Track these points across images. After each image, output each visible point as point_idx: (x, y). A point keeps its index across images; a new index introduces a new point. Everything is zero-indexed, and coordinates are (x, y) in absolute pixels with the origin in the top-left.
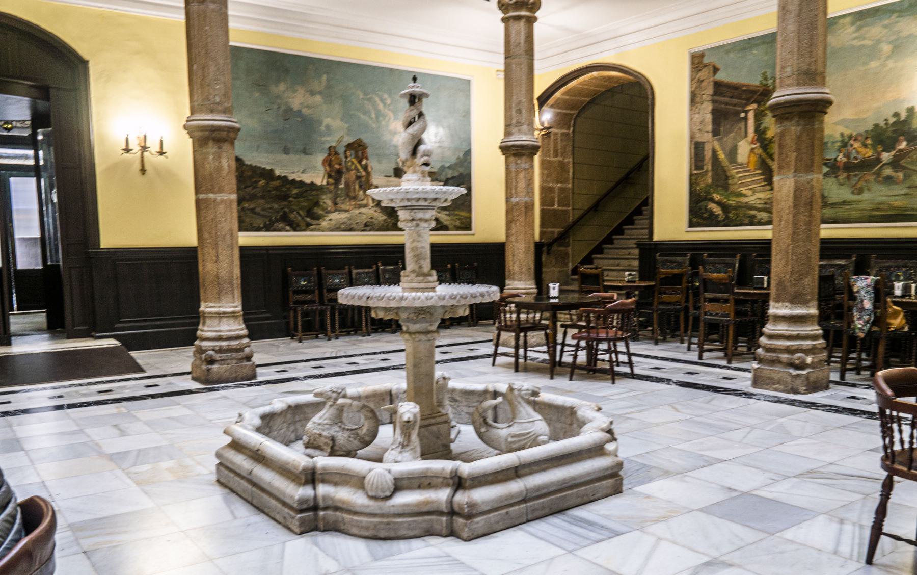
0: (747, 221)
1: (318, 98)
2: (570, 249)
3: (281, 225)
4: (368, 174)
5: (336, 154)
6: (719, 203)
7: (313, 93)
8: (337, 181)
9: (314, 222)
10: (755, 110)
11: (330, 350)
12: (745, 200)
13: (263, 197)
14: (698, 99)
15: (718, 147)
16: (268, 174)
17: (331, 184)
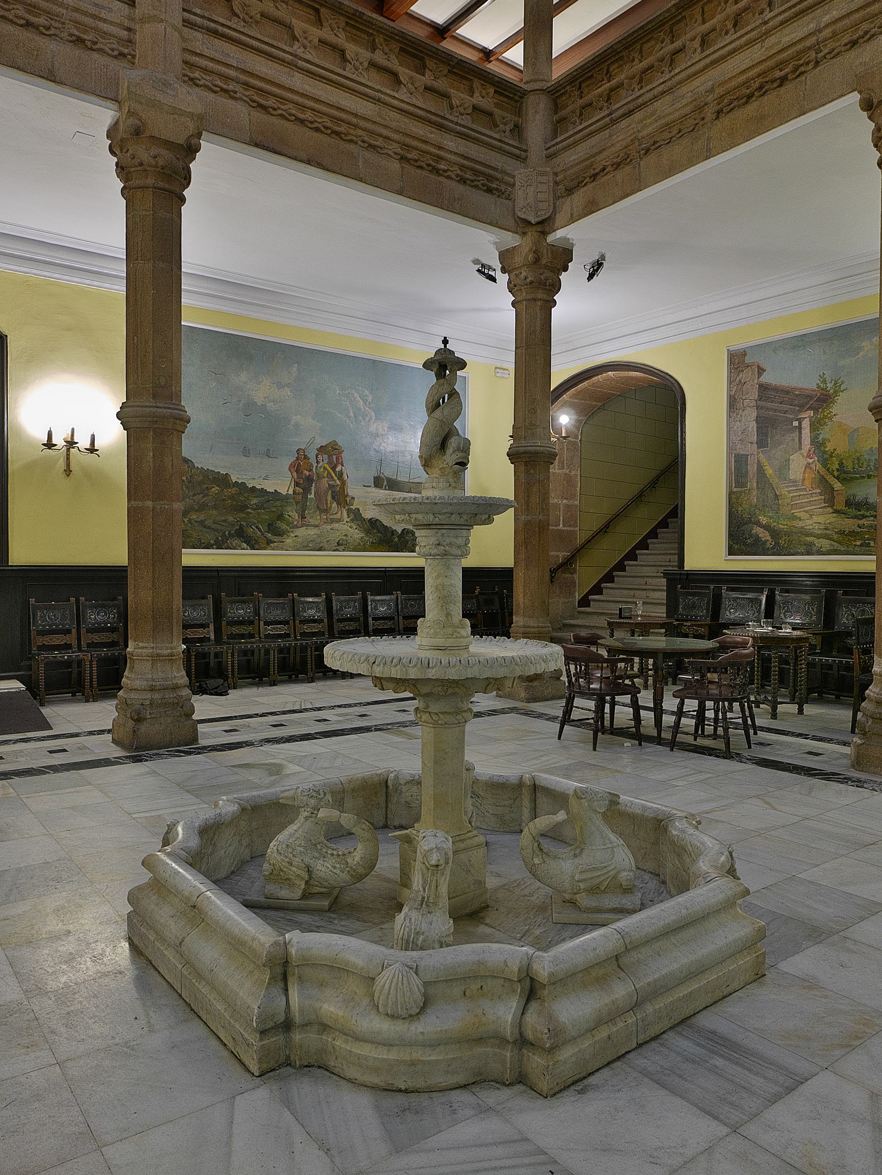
0: (802, 549)
1: (287, 391)
2: (576, 576)
3: (236, 542)
4: (344, 483)
5: (306, 457)
6: (767, 527)
7: (280, 386)
8: (306, 490)
9: (276, 539)
10: (810, 418)
11: (293, 699)
12: (801, 524)
13: (215, 507)
14: (739, 405)
15: (764, 461)
16: (223, 480)
17: (299, 494)
